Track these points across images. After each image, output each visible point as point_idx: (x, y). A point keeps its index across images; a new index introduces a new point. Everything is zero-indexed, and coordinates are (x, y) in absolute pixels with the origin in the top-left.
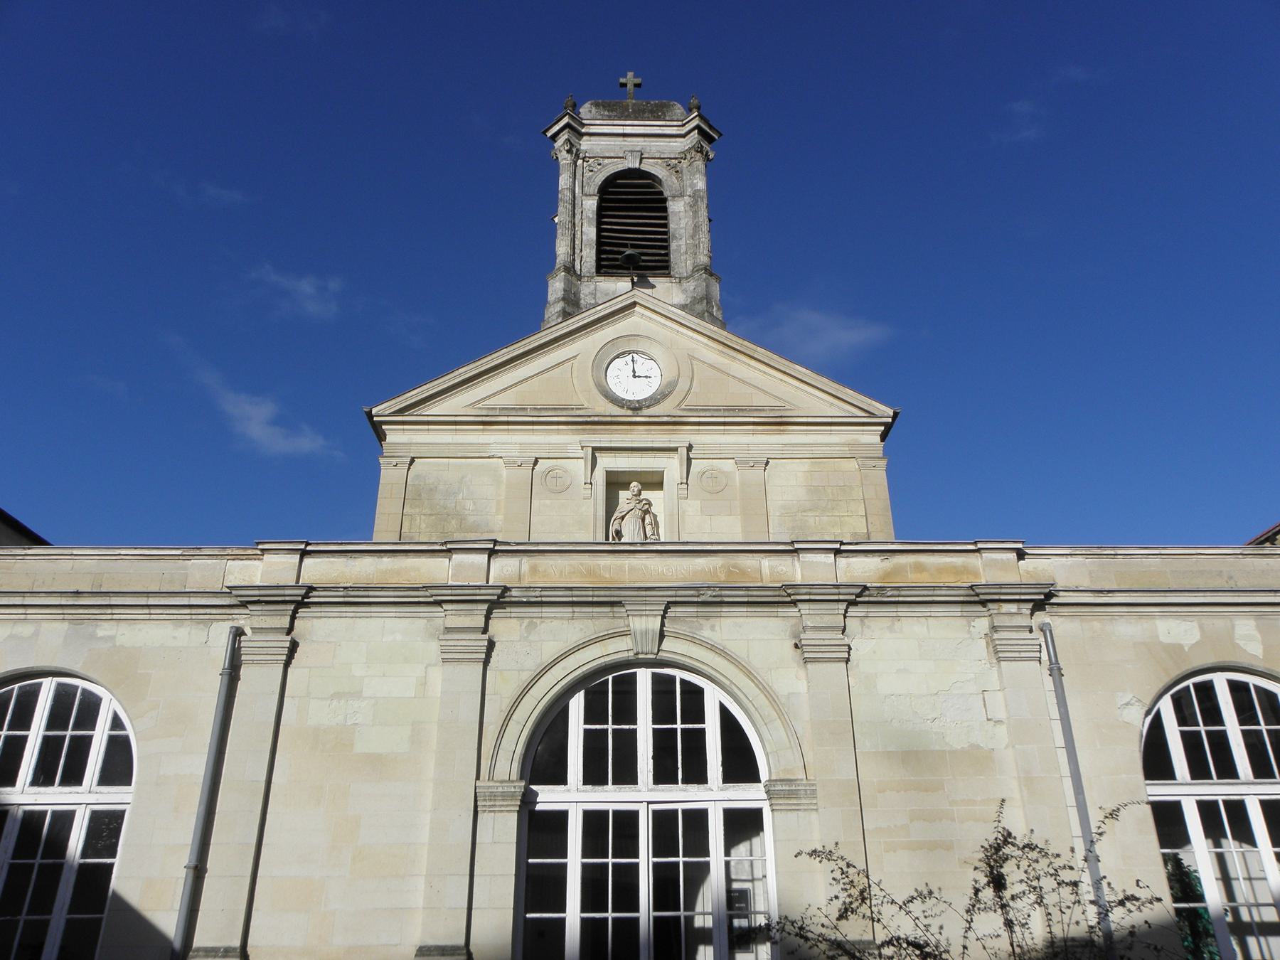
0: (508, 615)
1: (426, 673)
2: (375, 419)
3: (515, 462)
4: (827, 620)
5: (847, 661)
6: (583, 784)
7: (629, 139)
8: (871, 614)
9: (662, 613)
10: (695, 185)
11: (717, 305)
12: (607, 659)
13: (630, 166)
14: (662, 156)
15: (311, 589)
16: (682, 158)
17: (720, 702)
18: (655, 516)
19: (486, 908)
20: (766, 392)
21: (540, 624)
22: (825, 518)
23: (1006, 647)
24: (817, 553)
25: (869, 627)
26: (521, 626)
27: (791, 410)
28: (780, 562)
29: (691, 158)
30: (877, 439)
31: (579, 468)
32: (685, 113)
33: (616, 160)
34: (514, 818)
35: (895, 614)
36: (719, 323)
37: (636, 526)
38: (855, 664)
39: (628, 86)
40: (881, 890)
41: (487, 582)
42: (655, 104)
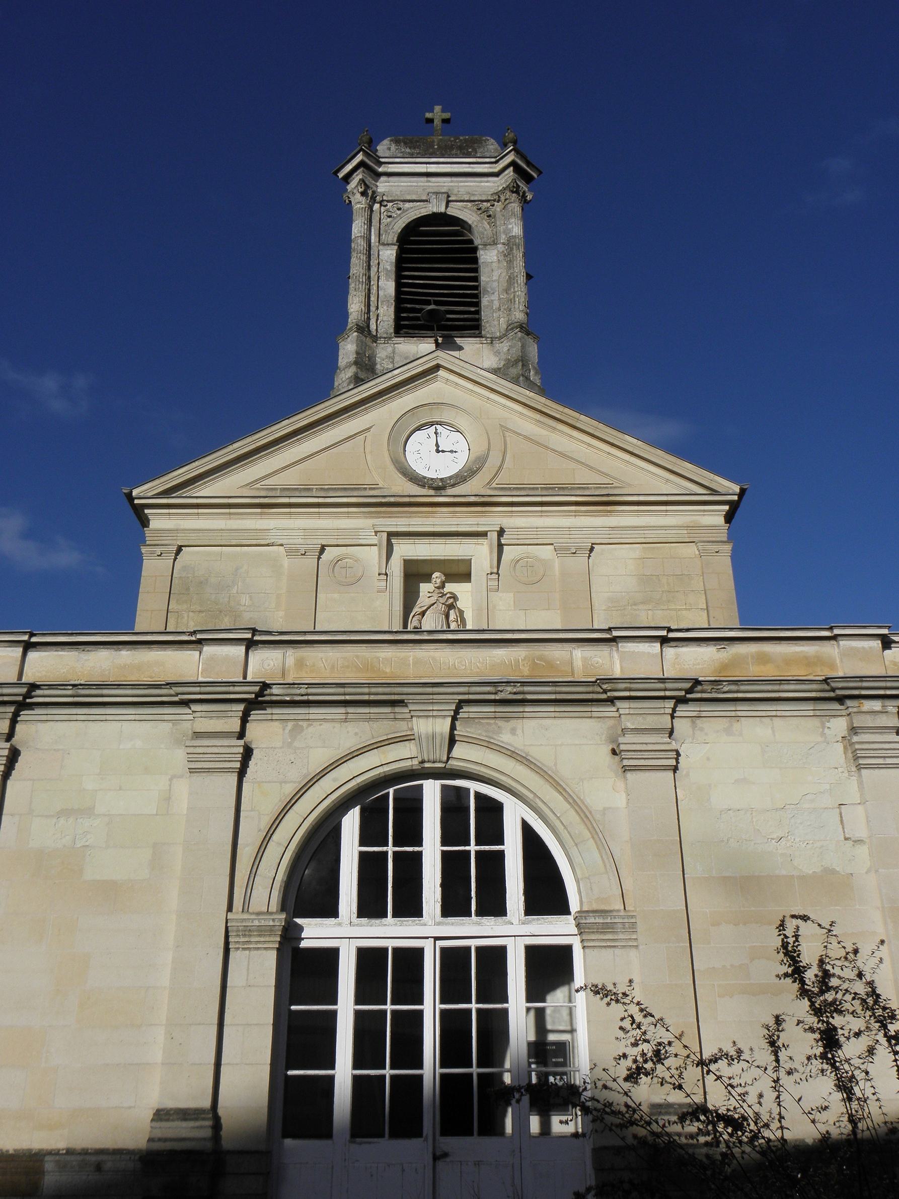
0: (269, 717)
1: (170, 786)
2: (136, 501)
3: (297, 550)
4: (650, 722)
5: (675, 769)
6: (358, 917)
7: (433, 179)
8: (704, 714)
9: (452, 713)
10: (510, 230)
11: (534, 368)
12: (386, 769)
13: (435, 210)
14: (472, 199)
15: (33, 687)
16: (494, 200)
17: (522, 818)
18: (461, 612)
19: (237, 1064)
20: (591, 468)
21: (307, 728)
22: (660, 612)
23: (867, 752)
24: (639, 642)
25: (702, 729)
26: (284, 730)
27: (619, 487)
28: (598, 653)
29: (506, 200)
30: (721, 520)
31: (372, 556)
32: (499, 148)
33: (418, 203)
34: (272, 957)
35: (733, 714)
36: (537, 388)
37: (439, 624)
38: (684, 773)
39: (436, 122)
40: (685, 1046)
41: (245, 677)
42: (465, 140)
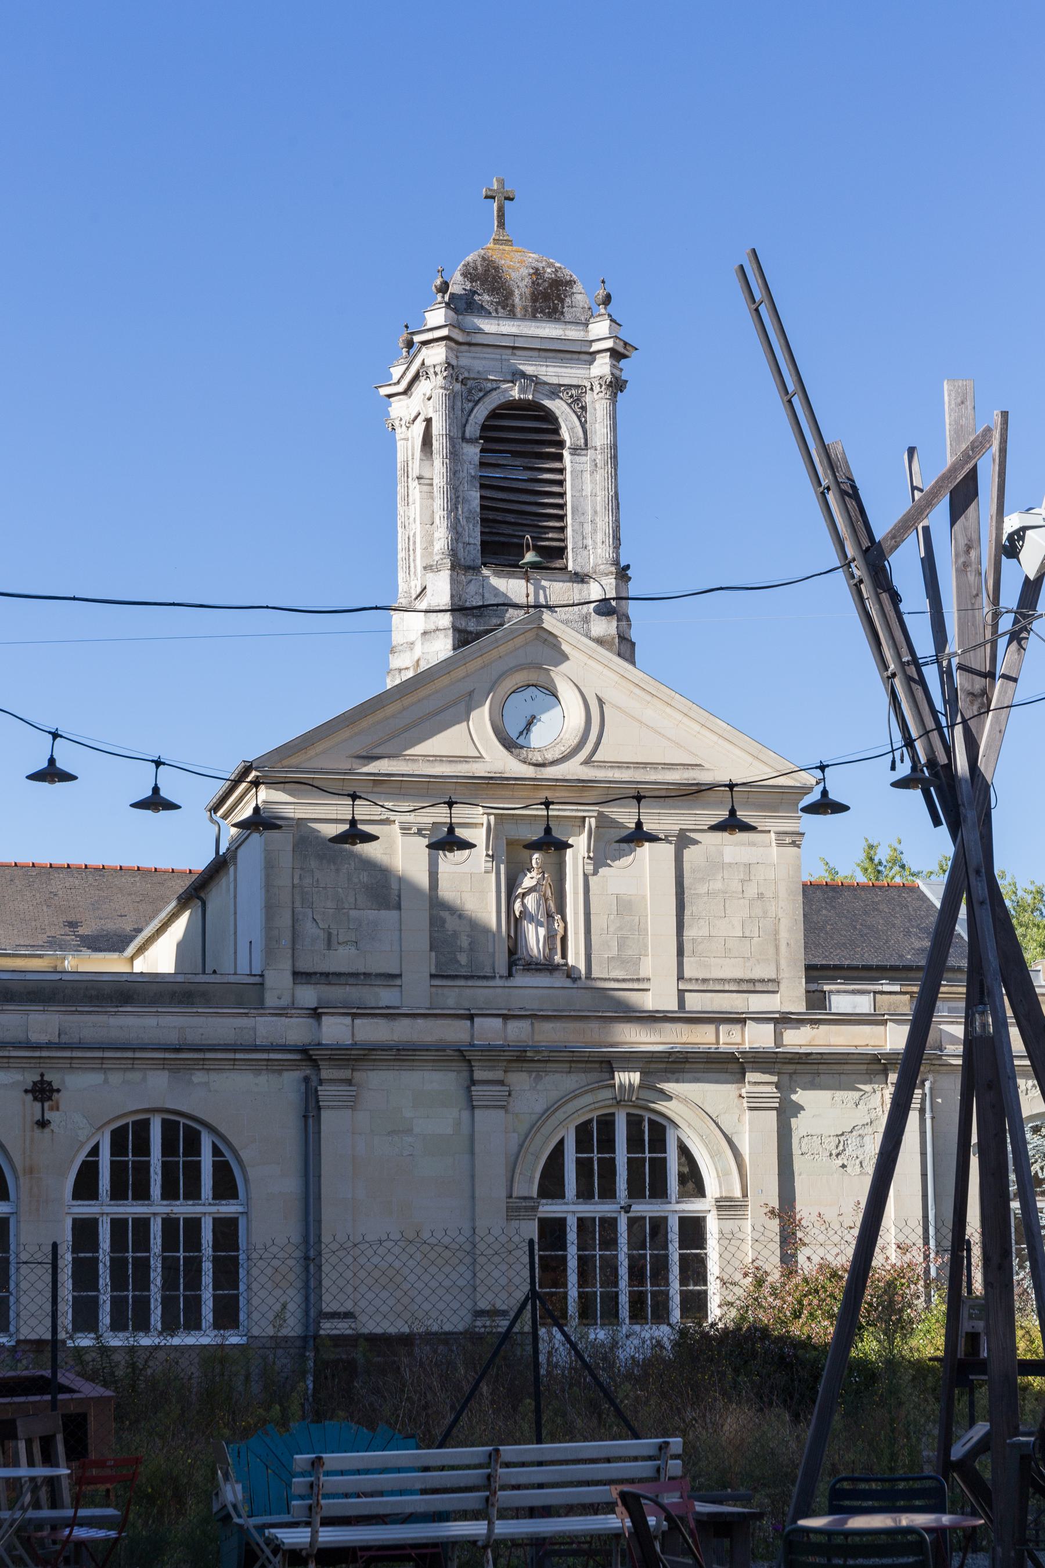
25: (796, 1081)
